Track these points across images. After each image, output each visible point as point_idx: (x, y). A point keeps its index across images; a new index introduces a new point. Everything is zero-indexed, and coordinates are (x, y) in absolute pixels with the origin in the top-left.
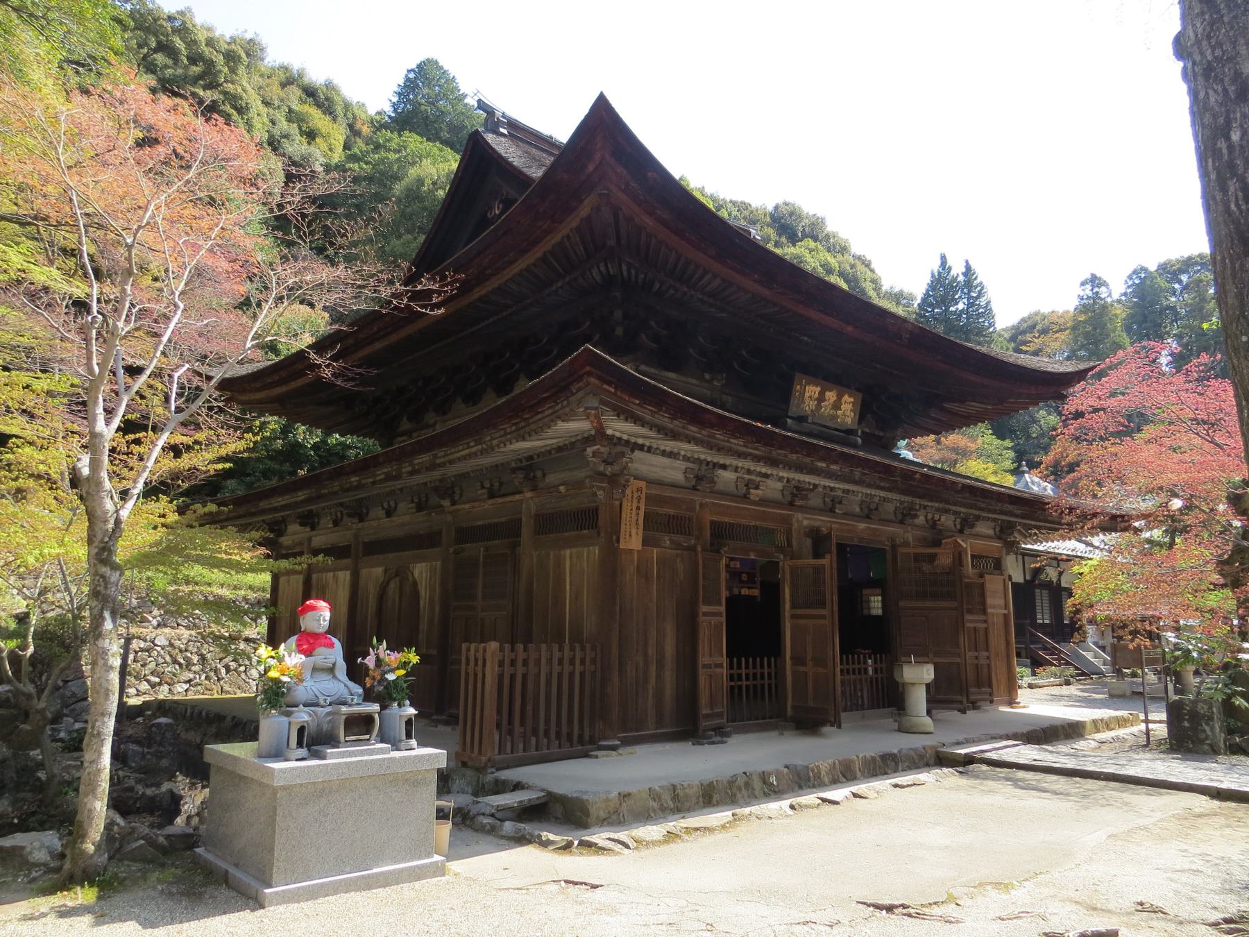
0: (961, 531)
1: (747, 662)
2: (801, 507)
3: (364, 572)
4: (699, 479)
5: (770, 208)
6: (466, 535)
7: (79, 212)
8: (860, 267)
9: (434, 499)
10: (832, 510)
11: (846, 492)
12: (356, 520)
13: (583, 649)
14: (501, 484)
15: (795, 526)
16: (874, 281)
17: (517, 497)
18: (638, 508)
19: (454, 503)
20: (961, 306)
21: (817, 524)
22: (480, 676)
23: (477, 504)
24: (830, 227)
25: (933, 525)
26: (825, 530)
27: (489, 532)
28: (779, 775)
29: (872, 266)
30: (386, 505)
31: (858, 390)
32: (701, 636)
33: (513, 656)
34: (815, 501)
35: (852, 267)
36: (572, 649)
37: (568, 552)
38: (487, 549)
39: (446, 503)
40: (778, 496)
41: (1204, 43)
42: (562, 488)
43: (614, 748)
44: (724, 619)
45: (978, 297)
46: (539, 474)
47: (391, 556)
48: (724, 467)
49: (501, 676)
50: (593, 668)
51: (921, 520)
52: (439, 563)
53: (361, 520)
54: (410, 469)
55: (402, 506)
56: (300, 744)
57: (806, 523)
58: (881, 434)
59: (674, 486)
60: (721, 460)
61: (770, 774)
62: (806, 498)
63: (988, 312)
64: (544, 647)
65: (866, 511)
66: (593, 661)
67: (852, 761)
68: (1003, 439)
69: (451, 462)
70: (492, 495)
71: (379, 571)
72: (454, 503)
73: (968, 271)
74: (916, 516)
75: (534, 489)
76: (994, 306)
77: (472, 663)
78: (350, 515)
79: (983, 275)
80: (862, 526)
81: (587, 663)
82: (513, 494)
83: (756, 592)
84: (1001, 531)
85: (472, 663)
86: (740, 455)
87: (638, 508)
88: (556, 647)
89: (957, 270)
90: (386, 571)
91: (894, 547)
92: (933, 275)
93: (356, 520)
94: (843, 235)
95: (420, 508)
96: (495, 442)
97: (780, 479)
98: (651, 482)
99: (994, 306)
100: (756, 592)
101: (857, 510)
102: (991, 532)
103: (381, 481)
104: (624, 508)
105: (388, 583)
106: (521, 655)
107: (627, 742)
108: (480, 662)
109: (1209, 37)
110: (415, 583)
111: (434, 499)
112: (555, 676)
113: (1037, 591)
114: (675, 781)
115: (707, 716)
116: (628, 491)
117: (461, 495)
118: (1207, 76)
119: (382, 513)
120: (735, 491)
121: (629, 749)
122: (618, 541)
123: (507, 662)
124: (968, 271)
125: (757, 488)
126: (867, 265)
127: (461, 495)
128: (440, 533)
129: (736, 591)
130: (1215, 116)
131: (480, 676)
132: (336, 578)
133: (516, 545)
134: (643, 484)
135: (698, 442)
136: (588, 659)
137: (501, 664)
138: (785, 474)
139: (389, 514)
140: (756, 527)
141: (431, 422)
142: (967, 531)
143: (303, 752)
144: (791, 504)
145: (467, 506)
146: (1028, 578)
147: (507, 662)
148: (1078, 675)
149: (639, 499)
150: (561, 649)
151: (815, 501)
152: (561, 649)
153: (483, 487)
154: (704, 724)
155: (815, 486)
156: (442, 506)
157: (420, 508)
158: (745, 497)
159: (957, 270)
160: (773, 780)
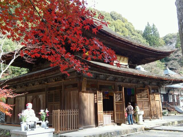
0: (149, 84)
1: (109, 112)
2: (117, 81)
3: (28, 97)
4: (97, 76)
5: (110, 13)
6: (50, 89)
7: (120, 120)
8: (130, 25)
9: (43, 82)
10: (123, 81)
11: (125, 78)
12: (26, 86)
13: (76, 110)
14: (57, 79)
15: (116, 85)
16: (133, 28)
17: (61, 81)
18: (85, 83)
19: (47, 83)
20: (152, 33)
21: (120, 84)
22: (56, 116)
23: (52, 83)
24: (123, 16)
25: (144, 83)
26: (122, 86)
27: (55, 88)
28: (113, 132)
29: (133, 25)
30: (32, 83)
31: (128, 57)
32: (98, 117)
33: (63, 112)
34: (119, 80)
35: (128, 25)
36: (74, 111)
37: (72, 92)
38: (55, 92)
39: (46, 83)
40: (112, 79)
41: (179, 5)
42: (70, 80)
43: (82, 129)
44: (102, 104)
45: (155, 31)
46: (65, 77)
47: (34, 93)
48: (101, 75)
49: (60, 116)
50: (78, 114)
51: (141, 82)
52: (45, 95)
53: (27, 86)
54: (40, 77)
55: (36, 83)
56: (29, 128)
57: (118, 84)
58: (133, 65)
59: (92, 78)
60: (101, 73)
61: (112, 132)
62: (117, 79)
63: (158, 35)
64: (64, 110)
65: (130, 81)
66: (78, 113)
67: (128, 130)
68: (162, 62)
69: (49, 75)
70: (56, 81)
71: (31, 97)
72: (47, 83)
73: (154, 25)
74: (140, 82)
75: (64, 80)
76: (159, 33)
77: (55, 114)
78: (24, 85)
79: (157, 27)
80: (129, 84)
81: (77, 113)
82: (61, 81)
83: (109, 98)
84: (158, 84)
85: (55, 114)
86: (104, 73)
87: (85, 83)
88: (70, 110)
89: (151, 25)
90: (33, 97)
91: (135, 88)
92: (146, 27)
93: (26, 86)
94: (126, 18)
95: (40, 84)
96: (58, 72)
97: (112, 76)
98: (87, 78)
99: (159, 33)
100: (109, 98)
101: (128, 81)
102: (156, 84)
103: (34, 79)
104: (83, 83)
105: (33, 99)
106: (64, 112)
107: (84, 128)
108: (56, 114)
109: (179, 4)
110: (40, 99)
111: (43, 82)
112: (72, 116)
113: (169, 96)
114: (94, 134)
115: (99, 123)
116: (83, 80)
117: (49, 81)
118: (179, 11)
119: (32, 85)
120: (103, 78)
121: (85, 129)
122: (81, 89)
123: (62, 113)
124: (154, 25)
125: (108, 78)
126: (131, 24)
127: (49, 81)
128: (45, 89)
129: (104, 98)
130: (180, 17)
131: (56, 116)
132: (21, 98)
133: (61, 91)
134: (86, 78)
135: (96, 71)
136: (77, 112)
137: (60, 114)
138: (113, 75)
139: (33, 85)
140: (108, 85)
141: (40, 65)
142: (151, 84)
143: (30, 129)
144: (115, 81)
145: (51, 83)
146: (167, 93)
147: (62, 113)
148: (178, 113)
149: (85, 81)
150: (71, 111)
151: (119, 80)
152: (71, 111)
153: (54, 79)
154: (99, 124)
155: (119, 77)
156: (45, 83)
157: (40, 84)
158: (106, 80)
159: (151, 25)
160: (113, 134)
